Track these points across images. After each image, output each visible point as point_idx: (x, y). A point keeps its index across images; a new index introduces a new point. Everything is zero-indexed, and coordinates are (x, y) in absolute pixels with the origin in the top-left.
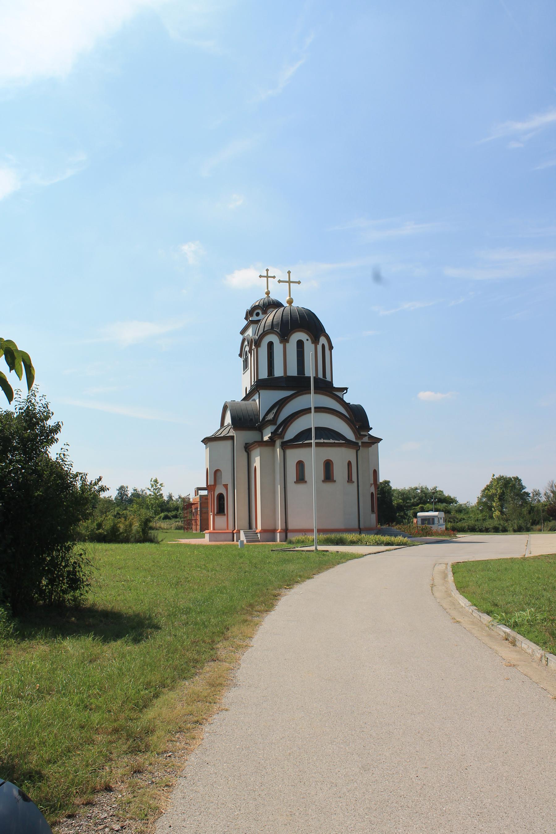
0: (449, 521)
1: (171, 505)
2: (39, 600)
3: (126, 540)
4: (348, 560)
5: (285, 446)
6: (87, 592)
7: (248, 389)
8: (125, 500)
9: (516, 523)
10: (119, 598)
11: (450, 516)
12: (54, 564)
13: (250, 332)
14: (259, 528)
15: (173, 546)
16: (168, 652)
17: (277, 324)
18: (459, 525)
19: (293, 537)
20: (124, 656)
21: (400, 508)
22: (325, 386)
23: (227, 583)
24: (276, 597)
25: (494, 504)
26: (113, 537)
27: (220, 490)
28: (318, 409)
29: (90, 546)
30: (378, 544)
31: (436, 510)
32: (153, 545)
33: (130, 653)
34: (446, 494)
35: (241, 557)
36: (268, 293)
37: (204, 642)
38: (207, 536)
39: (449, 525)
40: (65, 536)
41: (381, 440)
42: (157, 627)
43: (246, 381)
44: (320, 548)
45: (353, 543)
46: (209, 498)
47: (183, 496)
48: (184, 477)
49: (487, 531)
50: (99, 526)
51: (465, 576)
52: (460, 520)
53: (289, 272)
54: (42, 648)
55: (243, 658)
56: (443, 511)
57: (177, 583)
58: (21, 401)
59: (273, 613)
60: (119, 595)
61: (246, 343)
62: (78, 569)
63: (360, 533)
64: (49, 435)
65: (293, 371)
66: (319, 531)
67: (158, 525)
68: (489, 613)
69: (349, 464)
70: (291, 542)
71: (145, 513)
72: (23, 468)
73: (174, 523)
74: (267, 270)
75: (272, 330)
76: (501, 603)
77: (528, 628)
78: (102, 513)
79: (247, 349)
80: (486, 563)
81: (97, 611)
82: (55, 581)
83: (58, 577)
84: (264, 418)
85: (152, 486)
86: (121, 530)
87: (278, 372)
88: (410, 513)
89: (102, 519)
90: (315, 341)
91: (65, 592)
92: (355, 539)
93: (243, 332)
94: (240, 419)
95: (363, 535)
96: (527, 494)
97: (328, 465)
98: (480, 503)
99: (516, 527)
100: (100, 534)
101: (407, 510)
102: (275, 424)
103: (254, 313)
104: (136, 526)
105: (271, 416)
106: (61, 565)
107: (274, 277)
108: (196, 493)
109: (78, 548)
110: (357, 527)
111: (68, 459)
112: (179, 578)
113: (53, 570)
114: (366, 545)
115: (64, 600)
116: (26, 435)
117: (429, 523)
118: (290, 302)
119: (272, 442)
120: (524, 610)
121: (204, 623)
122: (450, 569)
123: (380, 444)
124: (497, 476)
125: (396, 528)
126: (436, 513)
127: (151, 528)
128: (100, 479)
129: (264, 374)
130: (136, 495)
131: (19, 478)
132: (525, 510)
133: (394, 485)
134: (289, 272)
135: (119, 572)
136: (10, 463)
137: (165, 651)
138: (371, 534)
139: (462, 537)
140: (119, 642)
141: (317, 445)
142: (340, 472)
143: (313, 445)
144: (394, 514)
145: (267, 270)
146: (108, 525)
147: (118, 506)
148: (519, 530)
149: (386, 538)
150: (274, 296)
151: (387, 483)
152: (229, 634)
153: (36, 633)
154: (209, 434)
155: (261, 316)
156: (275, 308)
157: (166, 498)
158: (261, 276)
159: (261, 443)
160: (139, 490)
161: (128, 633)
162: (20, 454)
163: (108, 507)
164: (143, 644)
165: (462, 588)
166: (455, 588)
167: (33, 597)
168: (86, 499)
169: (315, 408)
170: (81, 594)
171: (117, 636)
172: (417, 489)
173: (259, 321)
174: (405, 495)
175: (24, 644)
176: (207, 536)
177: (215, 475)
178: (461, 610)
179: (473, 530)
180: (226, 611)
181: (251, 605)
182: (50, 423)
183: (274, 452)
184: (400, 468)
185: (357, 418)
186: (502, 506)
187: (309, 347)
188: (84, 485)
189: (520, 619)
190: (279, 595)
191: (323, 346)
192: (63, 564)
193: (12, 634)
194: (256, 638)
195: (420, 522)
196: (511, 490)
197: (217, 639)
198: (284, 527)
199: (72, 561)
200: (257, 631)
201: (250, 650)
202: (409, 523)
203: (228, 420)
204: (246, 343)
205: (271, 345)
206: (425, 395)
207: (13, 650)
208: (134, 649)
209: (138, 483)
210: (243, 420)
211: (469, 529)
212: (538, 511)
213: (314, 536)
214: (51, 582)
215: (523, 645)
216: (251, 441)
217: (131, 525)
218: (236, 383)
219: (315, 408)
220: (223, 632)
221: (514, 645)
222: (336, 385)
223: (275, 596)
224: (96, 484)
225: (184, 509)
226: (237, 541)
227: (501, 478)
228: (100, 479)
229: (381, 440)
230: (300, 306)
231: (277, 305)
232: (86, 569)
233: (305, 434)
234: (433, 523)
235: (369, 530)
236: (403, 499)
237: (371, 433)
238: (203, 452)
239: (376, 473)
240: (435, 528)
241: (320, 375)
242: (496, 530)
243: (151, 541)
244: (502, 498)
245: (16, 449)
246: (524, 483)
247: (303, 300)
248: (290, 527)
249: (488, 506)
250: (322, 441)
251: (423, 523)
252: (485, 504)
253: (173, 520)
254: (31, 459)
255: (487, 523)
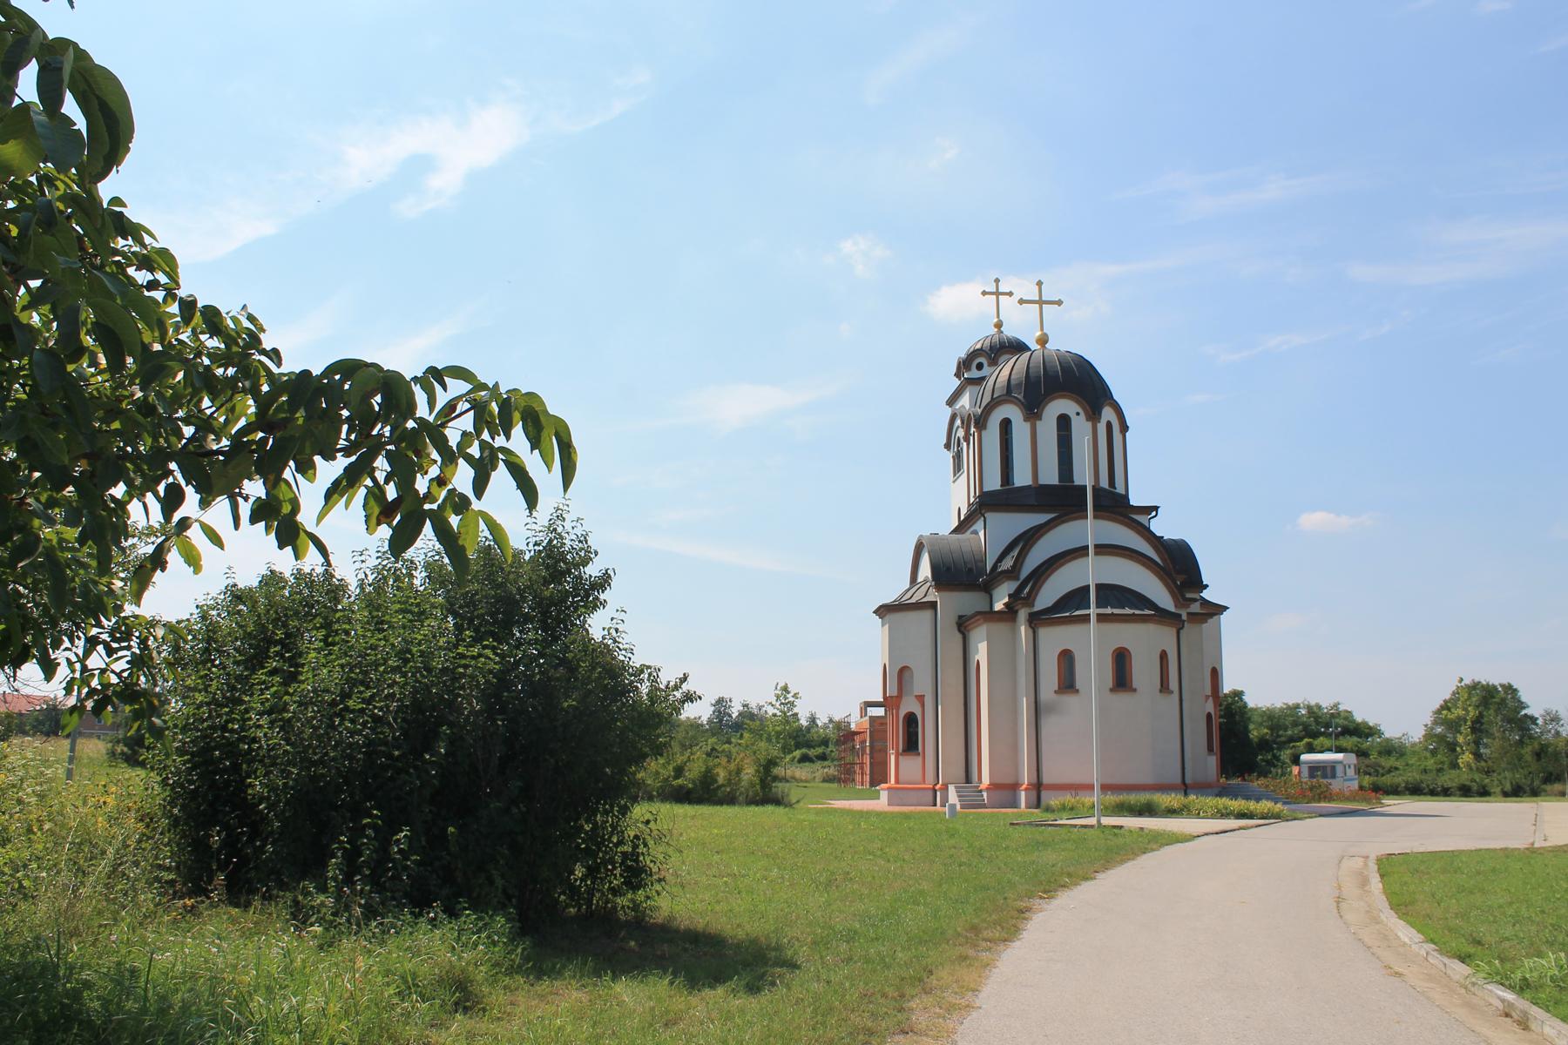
0: (1366, 773)
1: (813, 735)
2: (568, 906)
3: (730, 800)
4: (1162, 845)
5: (1036, 620)
6: (658, 893)
7: (964, 512)
8: (731, 726)
9: (1508, 778)
10: (718, 908)
11: (1367, 761)
12: (596, 837)
13: (965, 401)
14: (986, 780)
15: (818, 812)
16: (815, 1011)
17: (1019, 385)
18: (1387, 780)
19: (1051, 799)
20: (729, 1017)
21: (1264, 745)
22: (1114, 505)
23: (925, 886)
24: (1023, 913)
25: (1460, 739)
26: (704, 792)
27: (909, 705)
28: (1102, 549)
29: (665, 809)
30: (1224, 814)
31: (1339, 750)
32: (780, 810)
33: (742, 1011)
34: (1359, 718)
35: (952, 836)
36: (999, 325)
37: (884, 995)
38: (884, 795)
39: (1367, 780)
40: (621, 791)
41: (1226, 608)
42: (793, 966)
43: (959, 496)
44: (1106, 821)
45: (1171, 812)
46: (889, 720)
47: (836, 719)
48: (840, 680)
49: (1446, 793)
50: (679, 771)
51: (1406, 882)
52: (1389, 771)
53: (1040, 284)
54: (575, 994)
55: (961, 1029)
56: (1352, 751)
57: (829, 883)
58: (538, 528)
59: (1017, 944)
60: (718, 902)
61: (958, 422)
62: (641, 849)
63: (1186, 794)
64: (591, 593)
65: (1050, 476)
66: (1105, 788)
67: (789, 773)
68: (1464, 958)
69: (1163, 656)
70: (1048, 809)
71: (766, 749)
72: (541, 655)
73: (820, 770)
74: (997, 281)
75: (1008, 395)
76: (1489, 939)
77: (1555, 993)
78: (684, 747)
79: (961, 433)
80: (1454, 854)
81: (677, 931)
82: (598, 871)
83: (604, 863)
84: (995, 567)
85: (778, 697)
86: (721, 780)
87: (1022, 478)
88: (1285, 755)
89: (685, 758)
90: (1093, 415)
91: (615, 891)
92: (1176, 805)
93: (951, 401)
94: (949, 569)
95: (1192, 797)
96: (1533, 720)
97: (1121, 659)
98: (1429, 735)
99: (1508, 787)
100: (681, 787)
101: (1279, 749)
102: (1017, 578)
103: (972, 365)
104: (749, 773)
105: (1008, 563)
106: (609, 840)
107: (1010, 294)
108: (863, 713)
109: (639, 811)
110: (1178, 780)
111: (625, 640)
112: (833, 873)
113: (595, 852)
114: (1198, 816)
115: (614, 908)
116: (547, 594)
117: (1325, 776)
118: (1043, 341)
119: (1010, 613)
120: (1540, 955)
121: (883, 959)
122: (1373, 867)
123: (1224, 617)
124: (1467, 681)
125: (1257, 784)
126: (1340, 756)
127: (776, 779)
128: (684, 679)
129: (994, 483)
130: (748, 715)
131: (533, 675)
132: (1527, 751)
133: (1253, 700)
134: (1040, 284)
135: (716, 858)
136: (517, 647)
137: (809, 1010)
138: (1207, 795)
139: (1393, 804)
140: (720, 991)
141: (1102, 618)
142: (1144, 672)
143: (1093, 618)
144: (1247, 755)
145: (997, 281)
146: (694, 771)
147: (713, 735)
148: (1516, 792)
149: (1236, 804)
150: (1010, 331)
151: (1238, 694)
152: (933, 980)
153: (564, 967)
154: (889, 598)
155: (986, 370)
156: (1014, 354)
157: (804, 722)
158: (984, 293)
159: (990, 615)
160: (753, 705)
161: (737, 973)
162: (536, 629)
163: (694, 737)
164: (765, 997)
165: (1402, 906)
166: (1387, 904)
167: (557, 901)
168: (659, 715)
169: (1096, 546)
170: (648, 898)
171: (717, 979)
172: (1297, 706)
173: (983, 379)
174: (1275, 720)
175: (544, 986)
176: (884, 795)
177: (900, 676)
178: (1401, 950)
179: (1415, 790)
180: (926, 938)
181: (975, 929)
182: (592, 571)
183: (1015, 632)
184: (1263, 666)
185: (1179, 565)
186: (1477, 743)
187: (1081, 429)
188: (654, 689)
189: (1535, 974)
190: (1029, 909)
191: (1109, 425)
192: (615, 839)
193: (520, 966)
194: (987, 991)
195: (1305, 773)
196: (1497, 711)
197: (909, 991)
198: (1034, 780)
199: (632, 834)
200: (987, 977)
201: (974, 1014)
202: (1283, 774)
203: (925, 571)
204: (958, 422)
205: (1006, 425)
206: (1312, 520)
207: (521, 997)
208: (753, 1003)
209: (751, 691)
210: (954, 572)
211: (1407, 788)
212: (1556, 755)
213: (1095, 798)
214: (592, 872)
215: (1547, 1030)
216: (968, 612)
217: (739, 771)
218: (940, 500)
219: (1096, 546)
220: (921, 979)
221: (1526, 1028)
222: (1135, 500)
223: (1021, 911)
224: (676, 688)
225: (838, 743)
226: (943, 805)
227: (1475, 686)
228: (684, 679)
229: (1226, 608)
230: (1063, 349)
231: (1018, 347)
232: (657, 851)
233: (1077, 597)
234: (1334, 776)
235: (1202, 788)
236: (1271, 728)
237: (1205, 594)
238: (877, 632)
239: (1215, 674)
240: (1336, 785)
241: (1104, 483)
242: (1466, 792)
243: (777, 802)
244: (1478, 727)
245: (528, 618)
246: (1524, 697)
247: (1069, 335)
248: (1046, 780)
249: (1449, 744)
250: (1109, 610)
251: (1312, 776)
252: (1441, 738)
253: (819, 764)
254: (556, 639)
255: (1446, 777)
